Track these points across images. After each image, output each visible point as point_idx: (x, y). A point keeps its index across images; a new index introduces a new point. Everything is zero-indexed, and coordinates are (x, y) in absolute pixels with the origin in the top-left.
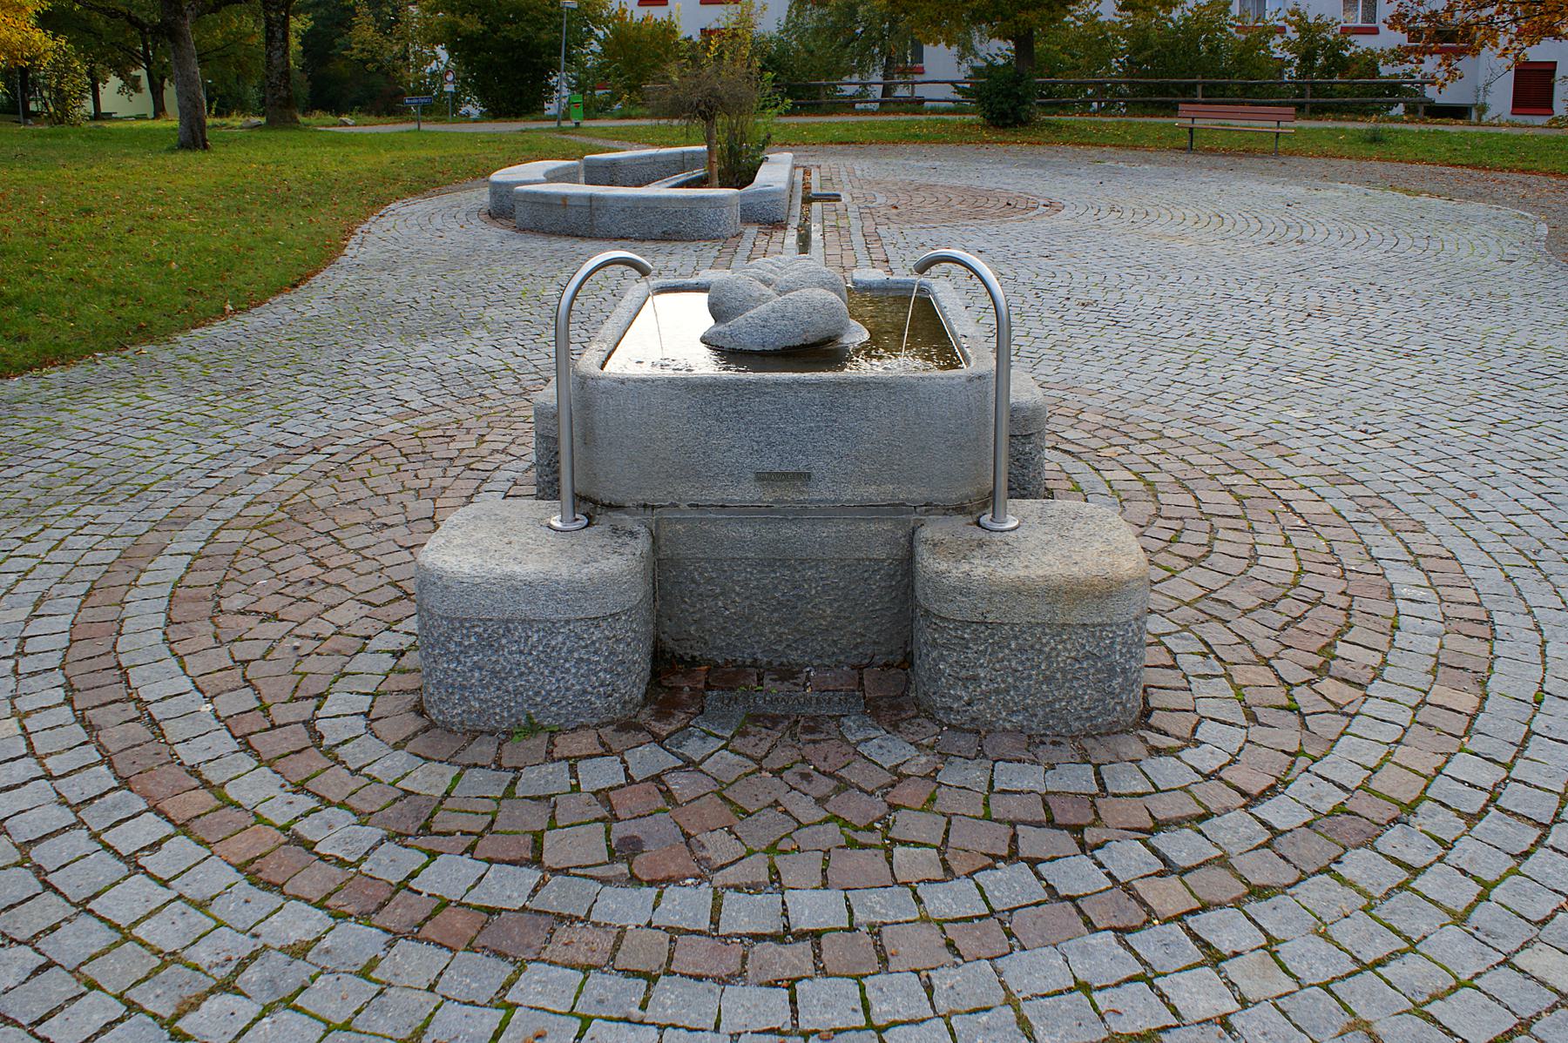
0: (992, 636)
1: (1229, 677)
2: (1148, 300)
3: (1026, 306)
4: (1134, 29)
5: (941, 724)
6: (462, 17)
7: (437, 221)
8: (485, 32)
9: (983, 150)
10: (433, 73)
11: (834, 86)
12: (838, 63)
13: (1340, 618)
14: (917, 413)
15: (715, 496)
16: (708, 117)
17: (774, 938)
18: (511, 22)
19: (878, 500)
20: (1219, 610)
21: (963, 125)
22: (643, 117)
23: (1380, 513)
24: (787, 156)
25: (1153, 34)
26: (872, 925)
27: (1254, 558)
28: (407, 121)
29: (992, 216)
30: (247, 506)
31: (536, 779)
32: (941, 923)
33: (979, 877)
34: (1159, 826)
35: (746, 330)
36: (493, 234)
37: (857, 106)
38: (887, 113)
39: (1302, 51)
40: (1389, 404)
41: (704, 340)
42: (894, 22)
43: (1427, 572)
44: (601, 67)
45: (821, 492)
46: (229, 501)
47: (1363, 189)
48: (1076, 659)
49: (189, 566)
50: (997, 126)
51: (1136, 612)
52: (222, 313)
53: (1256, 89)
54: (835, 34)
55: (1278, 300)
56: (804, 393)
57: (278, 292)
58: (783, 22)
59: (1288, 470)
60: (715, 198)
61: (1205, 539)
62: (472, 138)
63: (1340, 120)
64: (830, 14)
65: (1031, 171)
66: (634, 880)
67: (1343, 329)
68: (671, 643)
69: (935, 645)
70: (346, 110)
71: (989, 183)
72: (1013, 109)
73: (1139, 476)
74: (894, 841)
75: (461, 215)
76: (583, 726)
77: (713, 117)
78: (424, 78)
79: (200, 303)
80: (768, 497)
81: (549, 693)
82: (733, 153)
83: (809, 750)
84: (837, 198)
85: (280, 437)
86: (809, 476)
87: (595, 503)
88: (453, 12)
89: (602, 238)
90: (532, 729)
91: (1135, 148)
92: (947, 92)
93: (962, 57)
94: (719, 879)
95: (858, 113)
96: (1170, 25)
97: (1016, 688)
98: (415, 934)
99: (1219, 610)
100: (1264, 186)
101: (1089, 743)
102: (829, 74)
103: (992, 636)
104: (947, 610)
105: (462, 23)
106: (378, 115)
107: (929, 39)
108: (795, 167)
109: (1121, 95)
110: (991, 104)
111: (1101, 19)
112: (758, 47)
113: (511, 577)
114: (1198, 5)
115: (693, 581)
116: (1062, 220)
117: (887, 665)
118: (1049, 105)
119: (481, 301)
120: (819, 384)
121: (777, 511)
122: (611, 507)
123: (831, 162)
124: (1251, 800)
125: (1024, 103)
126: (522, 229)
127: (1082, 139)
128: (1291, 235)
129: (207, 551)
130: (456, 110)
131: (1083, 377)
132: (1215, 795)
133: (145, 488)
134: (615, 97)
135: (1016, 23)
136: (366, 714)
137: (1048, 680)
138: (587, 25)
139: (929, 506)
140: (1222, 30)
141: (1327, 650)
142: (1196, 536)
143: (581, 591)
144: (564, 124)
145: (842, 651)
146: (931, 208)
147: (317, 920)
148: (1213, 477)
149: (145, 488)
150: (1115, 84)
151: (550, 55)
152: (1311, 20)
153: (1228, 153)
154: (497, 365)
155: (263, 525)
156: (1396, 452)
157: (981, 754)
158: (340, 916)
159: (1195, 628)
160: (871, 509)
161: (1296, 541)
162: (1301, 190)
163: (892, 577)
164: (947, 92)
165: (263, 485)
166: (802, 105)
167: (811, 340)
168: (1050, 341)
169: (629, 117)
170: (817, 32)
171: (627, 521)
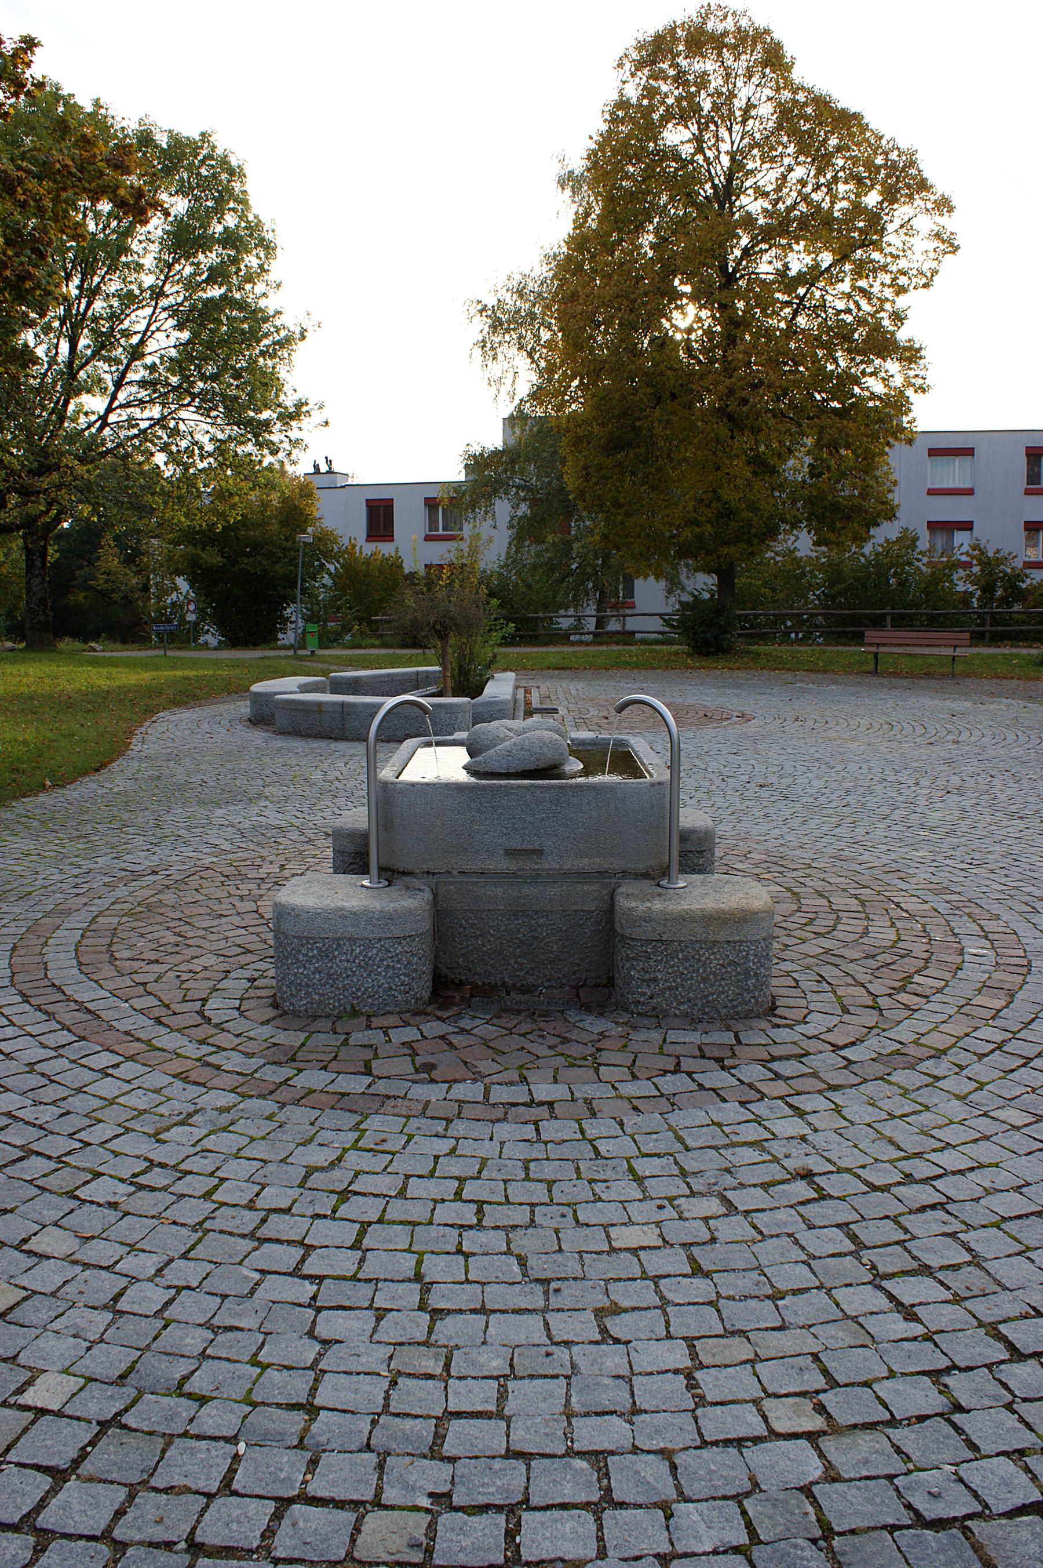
0: (666, 950)
1: (834, 992)
2: (815, 783)
3: (713, 788)
4: (830, 565)
5: (633, 1013)
6: (203, 549)
7: (205, 726)
8: (224, 565)
9: (687, 675)
10: (174, 604)
11: (551, 618)
12: (554, 597)
13: (922, 963)
14: (616, 808)
15: (476, 866)
16: (443, 637)
17: (524, 1104)
18: (248, 555)
19: (589, 869)
20: (833, 959)
21: (670, 654)
22: (373, 646)
23: (967, 910)
24: (511, 675)
25: (847, 569)
26: (586, 1099)
27: (866, 933)
28: (150, 648)
29: (690, 725)
30: (113, 904)
31: (359, 1037)
32: (629, 1099)
33: (654, 1080)
34: (774, 1059)
35: (492, 758)
36: (257, 737)
37: (572, 638)
38: (600, 644)
39: (983, 583)
40: (997, 848)
41: (464, 768)
42: (607, 557)
43: (992, 942)
44: (335, 599)
45: (550, 863)
46: (97, 901)
47: (1022, 703)
48: (723, 966)
49: (82, 936)
50: (700, 654)
51: (764, 935)
52: (43, 787)
53: (941, 619)
54: (552, 570)
55: (925, 782)
56: (538, 793)
57: (85, 773)
58: (502, 558)
59: (904, 886)
60: (451, 705)
61: (832, 923)
62: (217, 663)
63: (1017, 647)
64: (547, 550)
65: (728, 691)
66: (432, 1081)
67: (973, 801)
68: (445, 971)
69: (628, 959)
70: (95, 636)
71: (691, 701)
72: (716, 638)
73: (788, 889)
74: (600, 1065)
75: (224, 722)
76: (389, 1012)
77: (447, 635)
78: (165, 608)
79: (23, 779)
80: (513, 867)
81: (366, 989)
82: (463, 672)
83: (543, 1025)
84: (555, 711)
85: (123, 865)
86: (541, 852)
87: (393, 871)
88: (195, 545)
89: (352, 740)
90: (355, 1013)
91: (826, 672)
92: (656, 624)
93: (670, 592)
94: (487, 1080)
95: (573, 644)
96: (862, 559)
97: (682, 986)
98: (297, 1102)
99: (833, 959)
100: (936, 702)
101: (732, 1023)
102: (546, 608)
103: (666, 950)
104: (635, 933)
105: (204, 555)
106: (124, 641)
107: (639, 573)
108: (517, 687)
109: (817, 626)
110: (695, 634)
111: (798, 554)
112: (485, 580)
113: (342, 909)
114: (887, 541)
115: (461, 926)
116: (752, 728)
117: (597, 986)
118: (751, 635)
119: (260, 782)
120: (549, 787)
121: (520, 877)
122: (404, 873)
123: (548, 684)
124: (836, 1048)
125: (726, 632)
126: (283, 733)
127: (778, 665)
128: (950, 737)
129: (93, 927)
130: (195, 640)
131: (754, 832)
132: (813, 1045)
133: (30, 893)
134: (346, 628)
135: (718, 557)
136: (238, 1009)
137: (705, 980)
138: (319, 560)
139: (625, 874)
140: (910, 564)
141: (908, 979)
142: (823, 923)
143: (389, 918)
144: (300, 652)
145: (564, 976)
146: (637, 719)
147: (230, 1099)
148: (845, 890)
149: (30, 893)
150: (811, 615)
151: (284, 587)
152: (991, 554)
153: (910, 675)
154: (283, 823)
155: (130, 914)
156: (991, 876)
157: (659, 1026)
158: (245, 1096)
159: (816, 969)
160: (584, 875)
161: (899, 924)
162: (968, 704)
163: (599, 923)
164: (656, 624)
165: (121, 892)
166: (521, 637)
167: (542, 766)
168: (730, 810)
169: (360, 647)
170: (535, 567)
171: (415, 882)
